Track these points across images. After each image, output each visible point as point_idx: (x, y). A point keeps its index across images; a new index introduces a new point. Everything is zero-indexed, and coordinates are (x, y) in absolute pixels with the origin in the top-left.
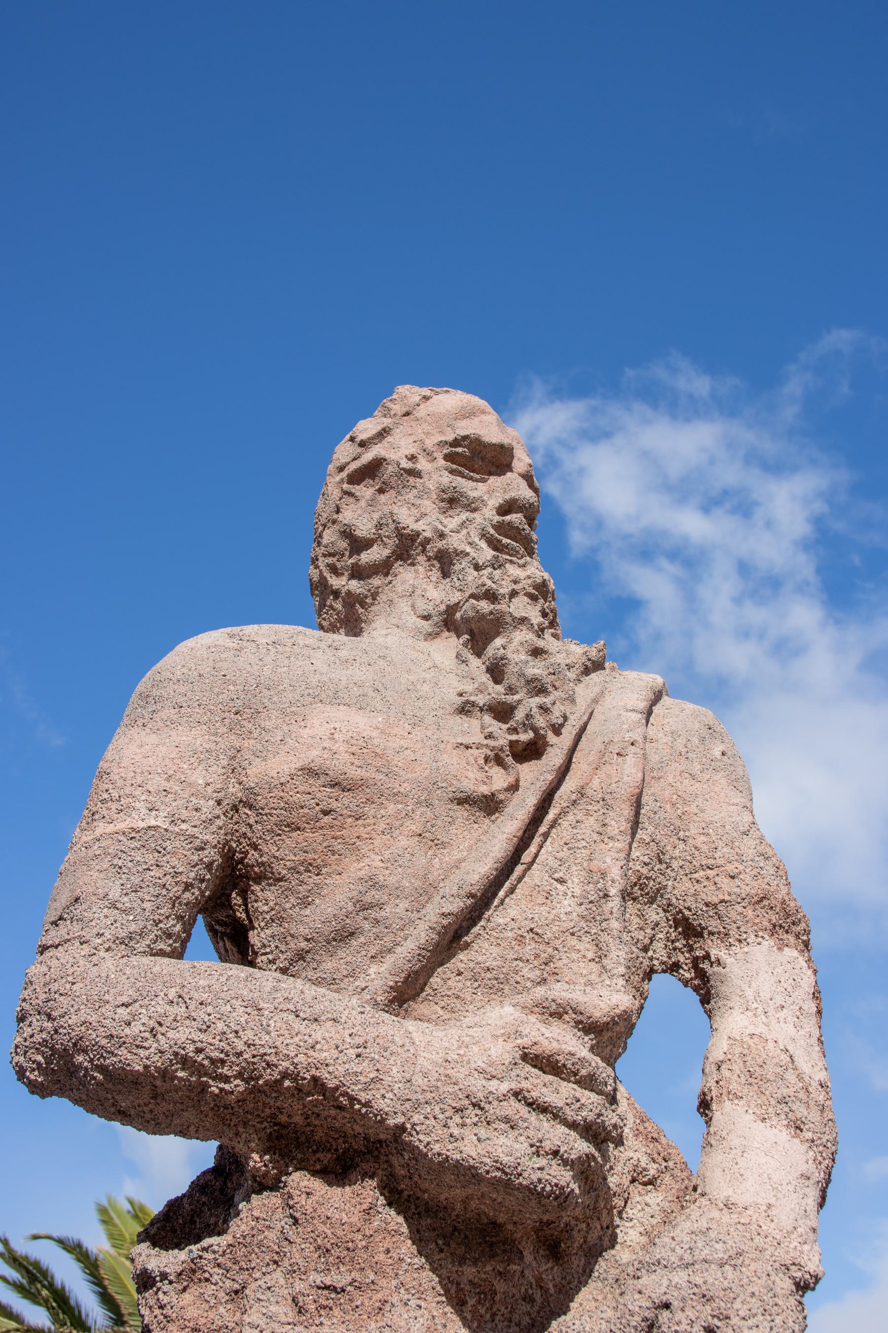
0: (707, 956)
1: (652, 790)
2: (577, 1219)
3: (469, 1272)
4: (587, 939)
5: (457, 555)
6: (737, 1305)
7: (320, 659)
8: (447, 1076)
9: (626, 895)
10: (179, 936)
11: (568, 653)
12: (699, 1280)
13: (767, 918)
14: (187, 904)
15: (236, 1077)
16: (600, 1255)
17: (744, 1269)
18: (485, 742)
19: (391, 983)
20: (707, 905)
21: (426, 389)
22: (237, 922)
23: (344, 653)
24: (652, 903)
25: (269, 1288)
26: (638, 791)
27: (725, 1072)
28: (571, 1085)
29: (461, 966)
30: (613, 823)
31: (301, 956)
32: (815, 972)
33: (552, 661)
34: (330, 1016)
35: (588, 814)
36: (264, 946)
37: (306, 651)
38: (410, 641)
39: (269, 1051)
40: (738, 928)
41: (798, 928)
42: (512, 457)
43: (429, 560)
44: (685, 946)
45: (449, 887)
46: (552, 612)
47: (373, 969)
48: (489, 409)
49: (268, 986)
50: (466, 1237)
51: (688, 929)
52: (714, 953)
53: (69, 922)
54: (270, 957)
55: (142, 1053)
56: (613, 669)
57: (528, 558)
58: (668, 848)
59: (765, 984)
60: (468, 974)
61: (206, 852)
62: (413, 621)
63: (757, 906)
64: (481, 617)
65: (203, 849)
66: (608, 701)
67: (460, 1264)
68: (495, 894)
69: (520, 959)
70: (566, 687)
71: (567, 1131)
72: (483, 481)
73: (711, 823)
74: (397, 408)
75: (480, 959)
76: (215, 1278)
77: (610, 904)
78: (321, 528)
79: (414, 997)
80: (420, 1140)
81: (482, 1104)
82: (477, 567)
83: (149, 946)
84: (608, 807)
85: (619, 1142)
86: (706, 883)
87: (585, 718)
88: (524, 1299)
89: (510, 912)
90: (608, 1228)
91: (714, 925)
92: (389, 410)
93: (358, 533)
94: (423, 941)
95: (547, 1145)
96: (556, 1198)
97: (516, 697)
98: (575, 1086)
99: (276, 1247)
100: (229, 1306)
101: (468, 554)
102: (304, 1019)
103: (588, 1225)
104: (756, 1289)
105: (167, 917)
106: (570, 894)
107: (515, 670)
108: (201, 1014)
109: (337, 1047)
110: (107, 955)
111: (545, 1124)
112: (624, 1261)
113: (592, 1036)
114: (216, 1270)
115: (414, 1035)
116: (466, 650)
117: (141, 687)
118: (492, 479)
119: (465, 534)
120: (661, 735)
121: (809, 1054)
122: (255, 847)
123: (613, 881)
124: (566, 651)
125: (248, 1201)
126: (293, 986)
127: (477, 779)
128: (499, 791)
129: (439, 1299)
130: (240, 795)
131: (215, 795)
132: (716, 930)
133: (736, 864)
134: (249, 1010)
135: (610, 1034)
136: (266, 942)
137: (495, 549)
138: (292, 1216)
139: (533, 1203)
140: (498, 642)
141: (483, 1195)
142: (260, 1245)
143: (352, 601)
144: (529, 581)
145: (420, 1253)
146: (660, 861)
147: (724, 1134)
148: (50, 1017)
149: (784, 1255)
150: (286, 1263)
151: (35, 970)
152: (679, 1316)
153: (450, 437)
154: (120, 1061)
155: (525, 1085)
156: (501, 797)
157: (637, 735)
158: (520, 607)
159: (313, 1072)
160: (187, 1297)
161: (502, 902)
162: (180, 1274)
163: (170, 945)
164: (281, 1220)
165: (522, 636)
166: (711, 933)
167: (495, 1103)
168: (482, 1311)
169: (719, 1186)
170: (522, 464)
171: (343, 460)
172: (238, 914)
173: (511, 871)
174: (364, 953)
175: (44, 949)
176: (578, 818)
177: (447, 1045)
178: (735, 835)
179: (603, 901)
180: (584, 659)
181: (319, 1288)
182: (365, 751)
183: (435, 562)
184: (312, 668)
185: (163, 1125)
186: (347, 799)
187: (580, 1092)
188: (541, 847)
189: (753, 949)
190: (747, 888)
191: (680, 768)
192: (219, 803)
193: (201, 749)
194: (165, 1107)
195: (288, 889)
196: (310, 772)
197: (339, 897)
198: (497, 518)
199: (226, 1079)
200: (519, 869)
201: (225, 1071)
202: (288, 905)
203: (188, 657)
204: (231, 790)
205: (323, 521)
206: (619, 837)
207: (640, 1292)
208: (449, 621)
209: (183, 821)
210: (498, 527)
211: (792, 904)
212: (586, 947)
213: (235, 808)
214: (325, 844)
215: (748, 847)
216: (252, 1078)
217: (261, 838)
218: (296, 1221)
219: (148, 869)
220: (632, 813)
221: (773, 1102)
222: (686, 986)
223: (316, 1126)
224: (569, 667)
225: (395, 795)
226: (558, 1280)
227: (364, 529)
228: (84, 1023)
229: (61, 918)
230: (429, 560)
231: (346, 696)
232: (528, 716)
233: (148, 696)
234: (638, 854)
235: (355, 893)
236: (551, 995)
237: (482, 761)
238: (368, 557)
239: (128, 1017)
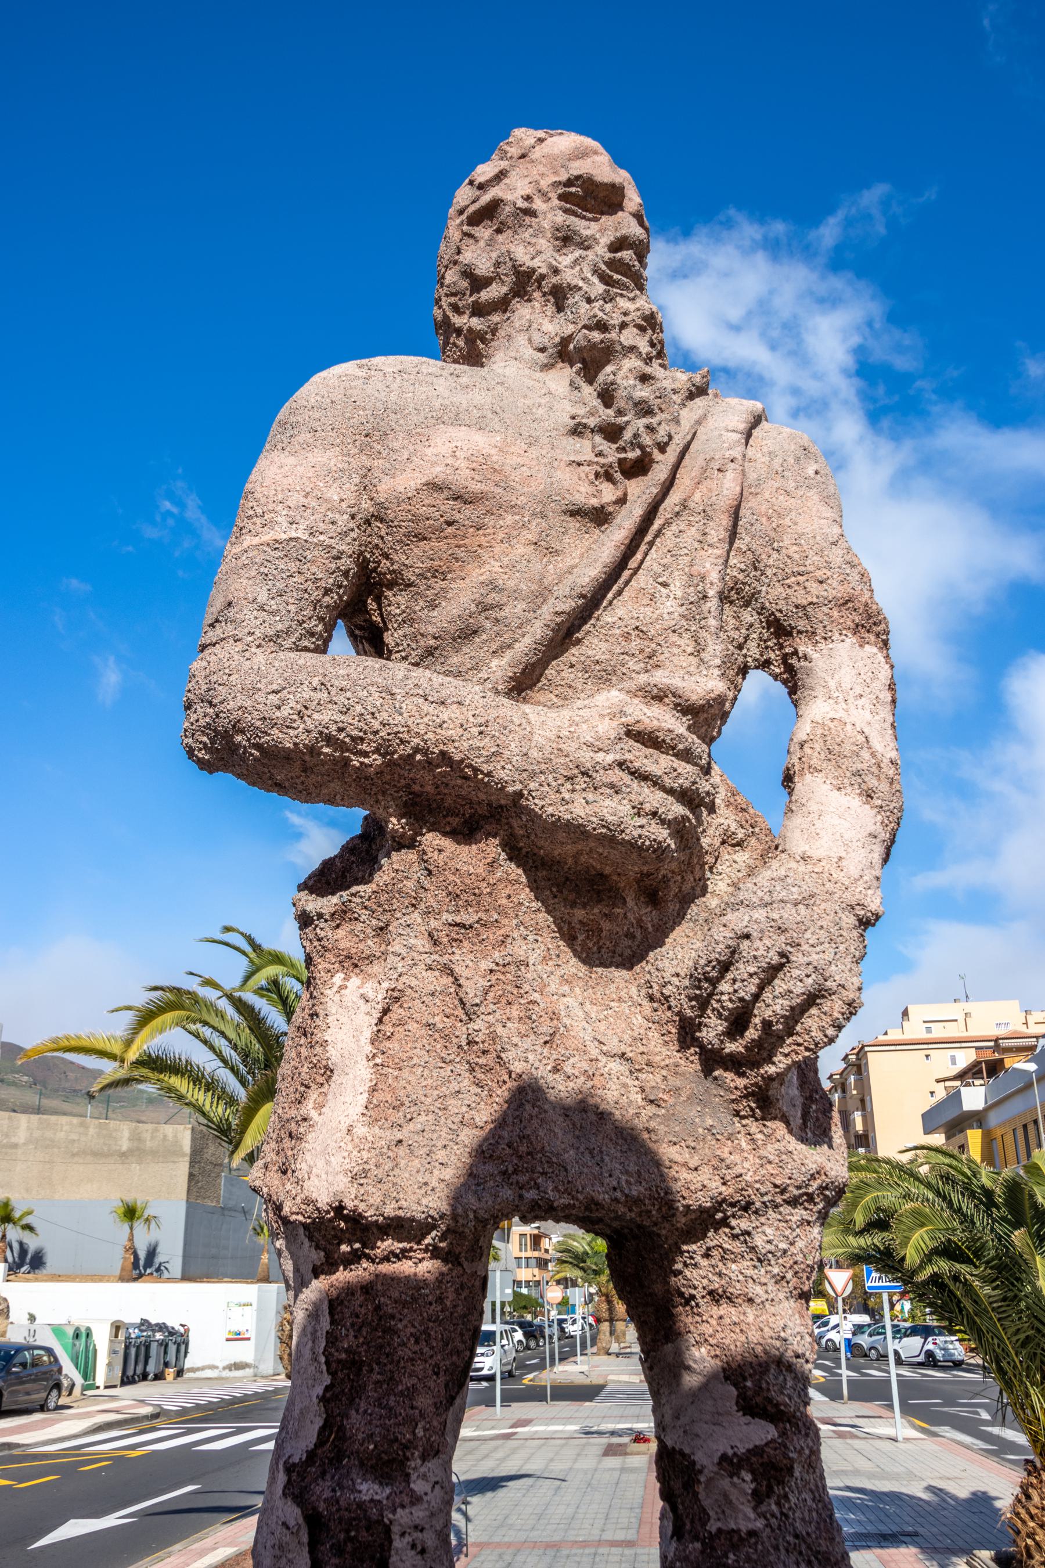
0: (795, 653)
1: (750, 504)
2: (673, 872)
3: (580, 913)
4: (688, 635)
5: (571, 289)
6: (808, 935)
7: (442, 386)
8: (559, 749)
9: (724, 598)
10: (321, 635)
11: (674, 379)
12: (776, 916)
13: (851, 618)
14: (327, 607)
15: (374, 752)
16: (693, 902)
17: (815, 908)
18: (596, 459)
19: (511, 674)
20: (797, 607)
21: (541, 131)
22: (373, 625)
23: (464, 380)
24: (747, 606)
25: (408, 926)
26: (736, 503)
27: (807, 750)
28: (669, 757)
29: (573, 659)
30: (713, 532)
31: (430, 652)
32: (892, 667)
33: (659, 385)
34: (455, 699)
35: (690, 524)
36: (398, 645)
37: (430, 379)
38: (527, 372)
39: (402, 730)
40: (825, 627)
41: (879, 629)
42: (623, 196)
43: (544, 296)
44: (776, 644)
45: (563, 590)
46: (660, 342)
47: (494, 663)
48: (601, 149)
49: (400, 675)
50: (577, 885)
51: (779, 629)
52: (801, 649)
53: (223, 624)
54: (403, 654)
55: (292, 732)
56: (716, 395)
57: (638, 292)
58: (763, 557)
59: (846, 676)
60: (580, 667)
61: (343, 561)
62: (529, 353)
63: (842, 608)
64: (593, 346)
65: (339, 558)
66: (711, 423)
67: (572, 908)
68: (604, 596)
69: (627, 653)
70: (671, 409)
71: (665, 796)
72: (596, 220)
73: (803, 534)
74: (513, 151)
75: (590, 653)
76: (363, 918)
77: (709, 604)
78: (443, 270)
79: (531, 687)
80: (535, 804)
81: (590, 773)
82: (589, 301)
83: (294, 643)
84: (709, 518)
85: (712, 809)
86: (796, 588)
87: (689, 437)
88: (626, 936)
89: (620, 611)
90: (700, 880)
91: (802, 624)
92: (506, 152)
93: (478, 272)
94: (538, 637)
95: (647, 807)
96: (655, 851)
97: (625, 419)
98: (673, 758)
99: (413, 894)
100: (375, 940)
101: (580, 288)
102: (432, 703)
103: (683, 877)
104: (824, 924)
105: (310, 618)
106: (672, 597)
107: (624, 394)
108: (341, 699)
109: (462, 726)
110: (258, 651)
111: (646, 790)
112: (713, 906)
113: (690, 717)
114: (364, 911)
115: (531, 716)
116: (579, 378)
117: (280, 416)
118: (604, 219)
119: (575, 269)
120: (760, 455)
121: (883, 736)
122: (387, 556)
123: (712, 584)
124: (672, 377)
125: (389, 857)
126: (421, 675)
127: (586, 492)
128: (608, 504)
129: (553, 935)
130: (371, 510)
131: (349, 510)
132: (804, 629)
133: (825, 571)
134: (383, 695)
135: (705, 715)
136: (399, 641)
137: (607, 284)
138: (426, 869)
139: (634, 856)
140: (609, 369)
141: (591, 850)
142: (400, 892)
143: (474, 337)
144: (638, 313)
145: (537, 899)
146: (756, 569)
147: (804, 801)
148: (211, 703)
149: (850, 898)
150: (423, 906)
151: (197, 665)
152: (758, 944)
153: (564, 177)
154: (273, 740)
155: (628, 756)
156: (611, 509)
157: (737, 452)
158: (629, 337)
159: (441, 747)
160: (341, 933)
161: (610, 603)
162: (333, 914)
163: (313, 643)
164: (417, 872)
165: (631, 363)
166: (800, 632)
167: (602, 772)
168: (590, 945)
169: (797, 844)
170: (632, 204)
171: (463, 204)
172: (374, 618)
173: (619, 576)
174: (486, 649)
175: (204, 647)
176: (681, 528)
177: (559, 724)
178: (825, 545)
179: (702, 602)
180: (689, 385)
181: (450, 925)
182: (485, 467)
183: (550, 297)
184: (435, 393)
185: (314, 795)
186: (468, 511)
187: (677, 763)
188: (646, 554)
189: (838, 646)
190: (834, 592)
191: (776, 485)
192: (353, 517)
193: (335, 468)
194: (314, 779)
195: (417, 593)
196: (435, 486)
197: (463, 600)
198: (609, 255)
199: (366, 754)
200: (626, 574)
201: (364, 747)
202: (417, 608)
203: (320, 387)
204: (363, 505)
205: (445, 262)
206: (718, 545)
207: (725, 926)
208: (563, 352)
209: (321, 533)
210: (611, 264)
211: (874, 607)
212: (686, 642)
213: (368, 522)
214: (450, 552)
215: (836, 556)
216: (387, 753)
217: (391, 548)
218: (430, 873)
219: (291, 576)
220: (730, 523)
221: (848, 774)
222: (776, 680)
223: (445, 794)
224: (675, 392)
225: (512, 507)
226: (655, 921)
227: (483, 267)
228: (241, 708)
229: (217, 621)
230: (544, 296)
231: (466, 418)
232: (636, 436)
233: (286, 423)
234: (735, 561)
235: (477, 596)
236: (653, 680)
237: (593, 477)
238: (486, 295)
239: (278, 702)
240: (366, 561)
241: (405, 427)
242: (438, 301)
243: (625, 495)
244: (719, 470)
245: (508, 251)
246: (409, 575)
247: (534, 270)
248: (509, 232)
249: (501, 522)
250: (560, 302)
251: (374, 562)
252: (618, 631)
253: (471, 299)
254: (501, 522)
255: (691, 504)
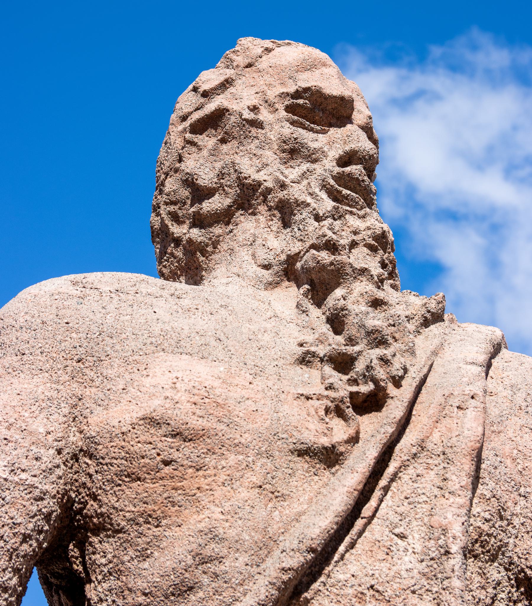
1: (493, 444)
5: (298, 205)
7: (163, 308)
9: (468, 553)
10: (15, 590)
18: (326, 393)
23: (186, 302)
24: (493, 561)
26: (478, 445)
30: (454, 478)
35: (428, 468)
37: (149, 300)
38: (251, 290)
43: (270, 210)
45: (290, 541)
46: (391, 263)
48: (330, 61)
56: (452, 321)
57: (368, 210)
58: (509, 504)
61: (45, 502)
62: (254, 270)
64: (322, 268)
65: (42, 499)
66: (447, 354)
68: (336, 549)
70: (406, 339)
72: (324, 132)
74: (240, 60)
77: (452, 562)
78: (163, 176)
82: (318, 218)
84: (449, 461)
87: (425, 370)
92: (232, 61)
93: (200, 182)
94: (263, 597)
97: (357, 348)
101: (308, 205)
106: (411, 550)
107: (355, 321)
116: (306, 301)
119: (305, 184)
120: (500, 388)
122: (94, 497)
123: (454, 538)
124: (406, 302)
128: (339, 443)
130: (80, 444)
131: (56, 443)
136: (102, 596)
137: (335, 199)
140: (339, 292)
143: (193, 249)
153: (292, 89)
156: (342, 449)
157: (477, 388)
158: (360, 258)
161: (342, 557)
163: (6, 600)
165: (362, 287)
170: (361, 116)
171: (186, 110)
172: (75, 567)
173: (352, 525)
176: (419, 472)
179: (444, 558)
182: (207, 400)
183: (276, 212)
184: (155, 316)
186: (187, 449)
188: (381, 501)
191: (520, 422)
192: (59, 452)
193: (42, 397)
195: (127, 541)
196: (152, 421)
200: (359, 523)
202: (126, 558)
203: (31, 305)
204: (72, 439)
205: (165, 169)
206: (460, 493)
208: (289, 271)
209: (23, 471)
210: (339, 178)
213: (75, 457)
214: (165, 495)
217: (101, 488)
220: (473, 468)
224: (409, 318)
227: (206, 177)
230: (270, 210)
231: (188, 345)
232: (369, 368)
234: (479, 510)
235: (195, 546)
237: (323, 413)
238: (209, 206)
240: (72, 501)
241: (121, 353)
242: (156, 208)
243: (358, 433)
244: (458, 407)
245: (233, 163)
246: (119, 520)
247: (259, 184)
248: (235, 143)
249: (223, 463)
250: (286, 218)
251: (80, 503)
252: (350, 591)
253: (192, 210)
254: (223, 463)
255: (430, 446)
